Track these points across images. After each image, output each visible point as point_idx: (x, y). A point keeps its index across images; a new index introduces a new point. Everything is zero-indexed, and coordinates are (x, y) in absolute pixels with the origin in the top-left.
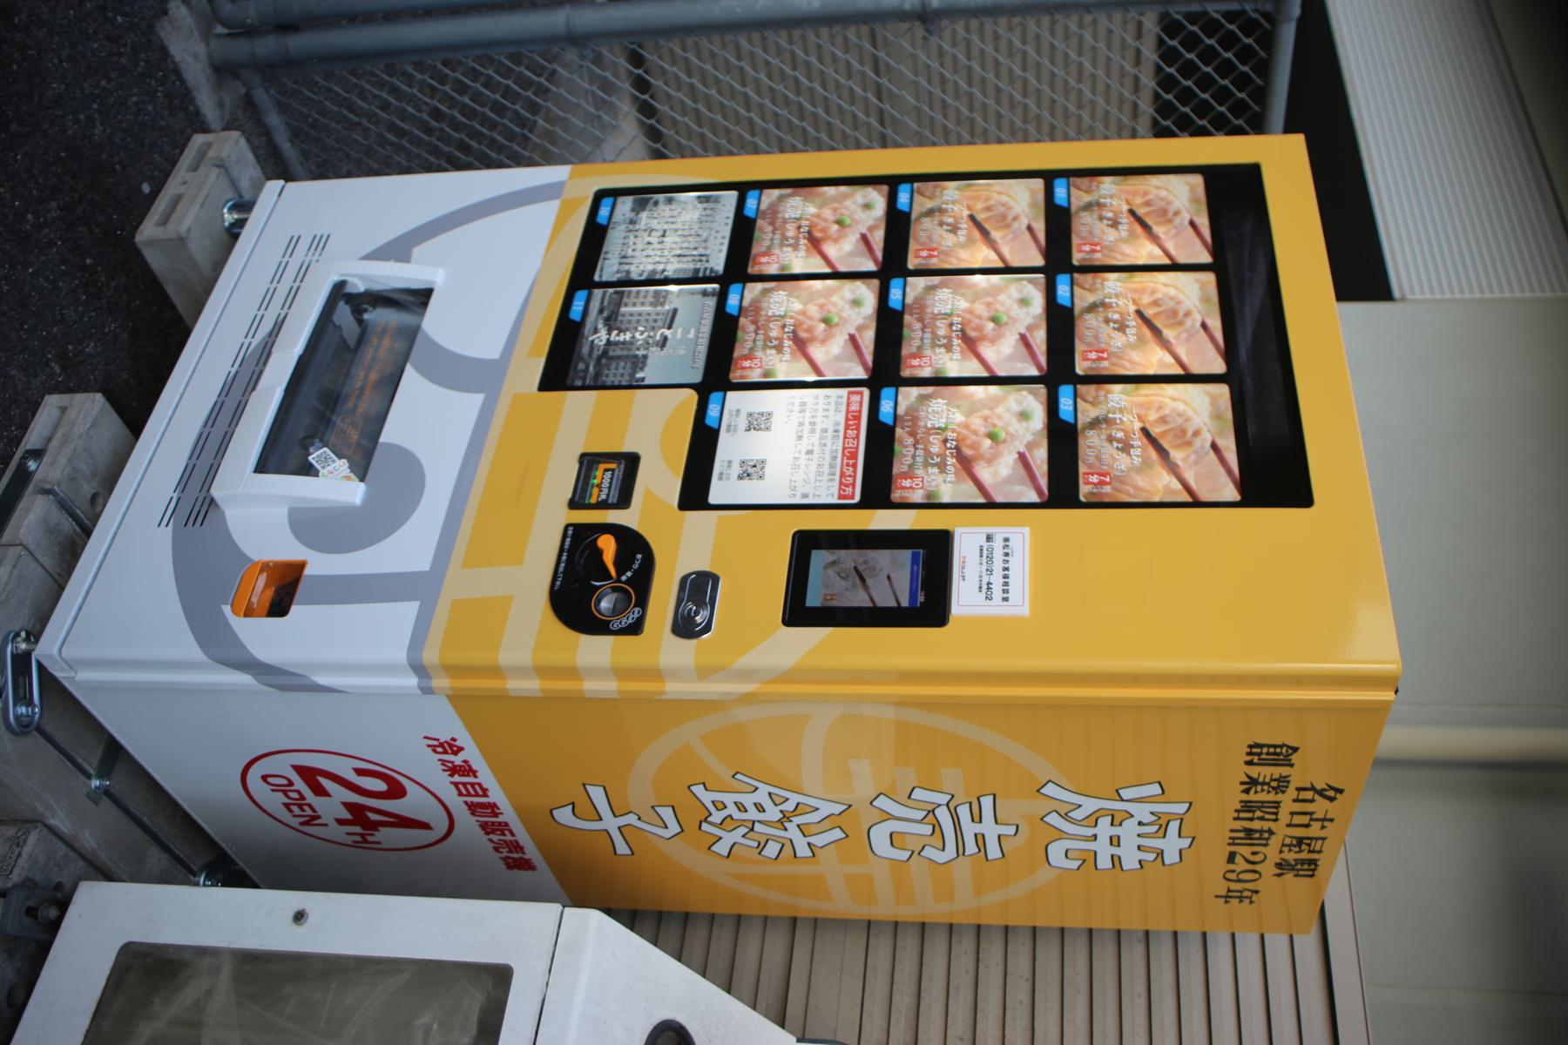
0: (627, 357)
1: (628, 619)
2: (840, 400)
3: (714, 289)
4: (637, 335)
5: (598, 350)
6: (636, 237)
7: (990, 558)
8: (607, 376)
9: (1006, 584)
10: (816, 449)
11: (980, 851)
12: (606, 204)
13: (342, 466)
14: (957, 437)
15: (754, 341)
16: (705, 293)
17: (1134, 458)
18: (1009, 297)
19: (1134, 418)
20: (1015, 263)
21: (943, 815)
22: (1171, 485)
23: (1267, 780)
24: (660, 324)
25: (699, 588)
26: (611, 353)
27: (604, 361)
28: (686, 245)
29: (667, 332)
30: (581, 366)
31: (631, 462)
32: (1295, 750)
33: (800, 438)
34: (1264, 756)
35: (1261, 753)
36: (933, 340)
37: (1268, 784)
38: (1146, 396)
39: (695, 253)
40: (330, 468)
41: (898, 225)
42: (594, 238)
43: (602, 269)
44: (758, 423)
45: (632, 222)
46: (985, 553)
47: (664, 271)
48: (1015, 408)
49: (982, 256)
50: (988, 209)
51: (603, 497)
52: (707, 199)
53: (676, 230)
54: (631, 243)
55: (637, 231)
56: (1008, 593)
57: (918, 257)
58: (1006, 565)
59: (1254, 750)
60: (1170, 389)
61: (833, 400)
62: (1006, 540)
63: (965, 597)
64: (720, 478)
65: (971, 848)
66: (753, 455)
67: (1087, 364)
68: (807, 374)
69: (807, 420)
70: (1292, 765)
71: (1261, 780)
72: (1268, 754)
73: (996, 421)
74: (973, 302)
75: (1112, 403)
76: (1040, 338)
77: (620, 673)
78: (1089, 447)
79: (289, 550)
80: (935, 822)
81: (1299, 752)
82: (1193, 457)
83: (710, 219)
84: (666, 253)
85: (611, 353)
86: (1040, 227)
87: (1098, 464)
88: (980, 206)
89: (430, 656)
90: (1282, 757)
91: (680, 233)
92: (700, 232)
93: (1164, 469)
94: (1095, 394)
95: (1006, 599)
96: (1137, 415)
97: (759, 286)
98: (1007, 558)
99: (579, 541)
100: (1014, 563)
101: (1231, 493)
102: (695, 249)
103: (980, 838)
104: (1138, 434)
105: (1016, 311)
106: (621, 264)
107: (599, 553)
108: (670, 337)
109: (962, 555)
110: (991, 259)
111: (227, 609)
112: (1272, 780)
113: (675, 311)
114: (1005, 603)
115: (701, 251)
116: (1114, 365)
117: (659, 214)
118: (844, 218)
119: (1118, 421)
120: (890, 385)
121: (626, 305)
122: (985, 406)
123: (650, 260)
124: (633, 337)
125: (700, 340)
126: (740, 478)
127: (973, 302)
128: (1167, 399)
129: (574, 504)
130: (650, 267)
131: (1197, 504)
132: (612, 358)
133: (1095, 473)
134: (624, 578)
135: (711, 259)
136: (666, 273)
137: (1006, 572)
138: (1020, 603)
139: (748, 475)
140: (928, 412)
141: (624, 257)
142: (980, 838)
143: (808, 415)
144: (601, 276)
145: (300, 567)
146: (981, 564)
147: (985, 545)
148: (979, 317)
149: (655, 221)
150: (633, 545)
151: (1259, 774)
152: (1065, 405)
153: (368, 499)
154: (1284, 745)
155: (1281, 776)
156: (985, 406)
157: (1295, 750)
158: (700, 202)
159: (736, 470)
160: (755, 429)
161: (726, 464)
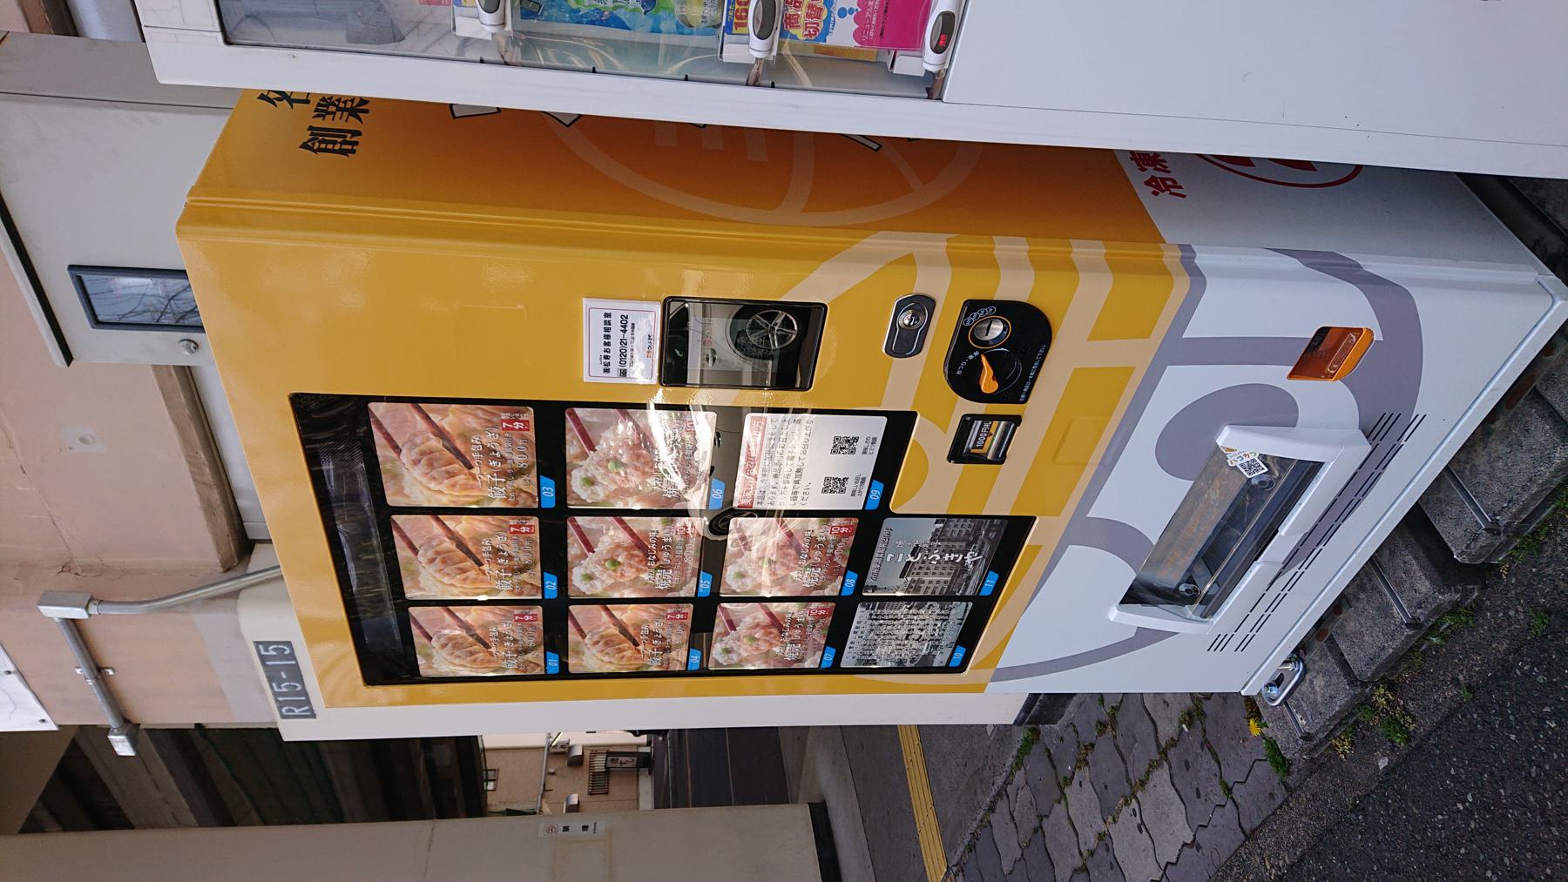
0: (948, 540)
1: (978, 316)
2: (760, 501)
3: (867, 592)
4: (938, 557)
5: (975, 547)
6: (932, 635)
8: (970, 526)
9: (607, 330)
10: (785, 461)
12: (955, 663)
13: (1234, 460)
15: (835, 548)
16: (875, 588)
17: (479, 443)
23: (339, 113)
24: (917, 566)
25: (904, 343)
26: (964, 544)
27: (971, 538)
28: (889, 628)
29: (911, 559)
30: (992, 535)
31: (959, 453)
32: (304, 146)
33: (799, 471)
34: (339, 140)
35: (341, 143)
37: (339, 109)
38: (468, 496)
39: (882, 622)
40: (1246, 459)
41: (837, 636)
42: (969, 636)
44: (835, 485)
45: (936, 647)
47: (910, 609)
48: (598, 489)
49: (627, 614)
51: (986, 425)
52: (868, 662)
53: (897, 639)
54: (937, 630)
55: (931, 640)
56: (605, 321)
57: (686, 614)
58: (607, 347)
59: (349, 147)
60: (444, 501)
61: (767, 500)
62: (607, 371)
63: (649, 322)
70: (311, 128)
71: (346, 114)
72: (335, 142)
74: (637, 578)
75: (502, 490)
76: (574, 548)
77: (992, 264)
78: (524, 453)
79: (1306, 392)
81: (301, 143)
83: (866, 647)
84: (907, 622)
85: (964, 544)
86: (573, 636)
88: (628, 653)
89: (1182, 286)
90: (320, 138)
91: (894, 637)
92: (876, 637)
93: (448, 432)
94: (518, 499)
95: (607, 315)
97: (827, 592)
98: (606, 354)
99: (1016, 386)
100: (599, 349)
101: (377, 409)
102: (881, 625)
104: (475, 463)
105: (597, 571)
106: (948, 615)
107: (996, 377)
108: (909, 555)
109: (650, 359)
110: (617, 611)
111: (1378, 336)
112: (334, 113)
113: (902, 576)
114: (608, 312)
115: (876, 623)
117: (910, 652)
119: (495, 475)
120: (871, 511)
121: (945, 582)
123: (922, 617)
124: (941, 556)
125: (882, 551)
126: (856, 439)
129: (1016, 420)
130: (922, 611)
131: (414, 401)
132: (963, 540)
134: (976, 354)
135: (868, 617)
136: (908, 606)
137: (607, 341)
138: (592, 311)
139: (849, 441)
141: (944, 620)
144: (967, 606)
145: (1292, 375)
148: (631, 566)
149: (914, 647)
150: (965, 382)
151: (347, 121)
152: (550, 490)
153: (1216, 430)
154: (315, 151)
155: (324, 116)
157: (304, 146)
158: (874, 660)
159: (859, 446)
160: (839, 480)
161: (868, 451)
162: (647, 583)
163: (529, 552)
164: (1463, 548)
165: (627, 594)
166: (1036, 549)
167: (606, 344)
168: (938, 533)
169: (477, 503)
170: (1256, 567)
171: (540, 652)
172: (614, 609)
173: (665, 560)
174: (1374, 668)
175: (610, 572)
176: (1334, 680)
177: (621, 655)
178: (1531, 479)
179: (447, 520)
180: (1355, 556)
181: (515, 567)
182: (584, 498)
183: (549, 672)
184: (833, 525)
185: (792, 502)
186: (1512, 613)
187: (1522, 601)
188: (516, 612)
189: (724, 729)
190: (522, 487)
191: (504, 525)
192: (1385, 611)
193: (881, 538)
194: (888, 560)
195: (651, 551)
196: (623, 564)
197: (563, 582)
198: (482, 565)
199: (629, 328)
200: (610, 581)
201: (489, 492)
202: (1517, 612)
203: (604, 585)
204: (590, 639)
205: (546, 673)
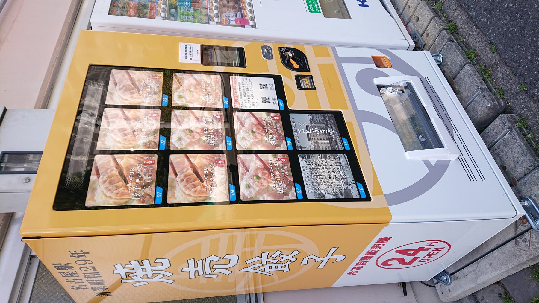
7: (190, 54)
11: (197, 262)
14: (203, 132)
17: (133, 171)
18: (185, 141)
19: (130, 189)
20: (182, 156)
21: (208, 271)
22: (128, 112)
36: (212, 86)
43: (347, 161)
46: (192, 56)
50: (195, 186)
62: (186, 58)
64: (272, 85)
65: (200, 263)
66: (264, 90)
67: (153, 159)
68: (254, 113)
69: (251, 99)
73: (190, 137)
74: (200, 139)
75: (138, 195)
78: (151, 175)
80: (211, 269)
82: (109, 171)
86: (171, 175)
87: (148, 168)
91: (324, 177)
94: (150, 145)
96: (135, 137)
102: (314, 168)
103: (196, 266)
107: (297, 64)
116: (142, 158)
118: (252, 134)
119: (147, 93)
122: (194, 142)
127: (200, 139)
128: (113, 197)
133: (150, 164)
139: (265, 85)
140: (213, 99)
142: (196, 266)
143: (251, 101)
146: (193, 53)
147: (192, 57)
149: (336, 183)
156: (194, 142)
162: (204, 142)
163: (150, 176)
164: (486, 100)
165: (197, 148)
166: (351, 123)
167: (186, 52)
168: (312, 120)
169: (133, 147)
170: (432, 120)
171: (153, 186)
172: (191, 157)
173: (211, 130)
174: (529, 154)
175: (188, 136)
176: (534, 179)
177: (195, 189)
178: (471, 76)
179: (125, 110)
180: (469, 127)
181: (143, 184)
182: (177, 147)
183: (156, 203)
184: (279, 157)
185: (253, 106)
186: (522, 101)
187: (518, 97)
188: (154, 75)
189: (248, 154)
190: (156, 98)
191: (142, 160)
192: (506, 142)
193: (292, 123)
194: (299, 132)
195: (203, 87)
196: (193, 92)
197: (170, 100)
198: (140, 91)
199: (192, 48)
200: (188, 141)
201: (132, 196)
202: (521, 99)
203: (186, 143)
204: (180, 177)
205: (162, 106)
